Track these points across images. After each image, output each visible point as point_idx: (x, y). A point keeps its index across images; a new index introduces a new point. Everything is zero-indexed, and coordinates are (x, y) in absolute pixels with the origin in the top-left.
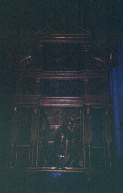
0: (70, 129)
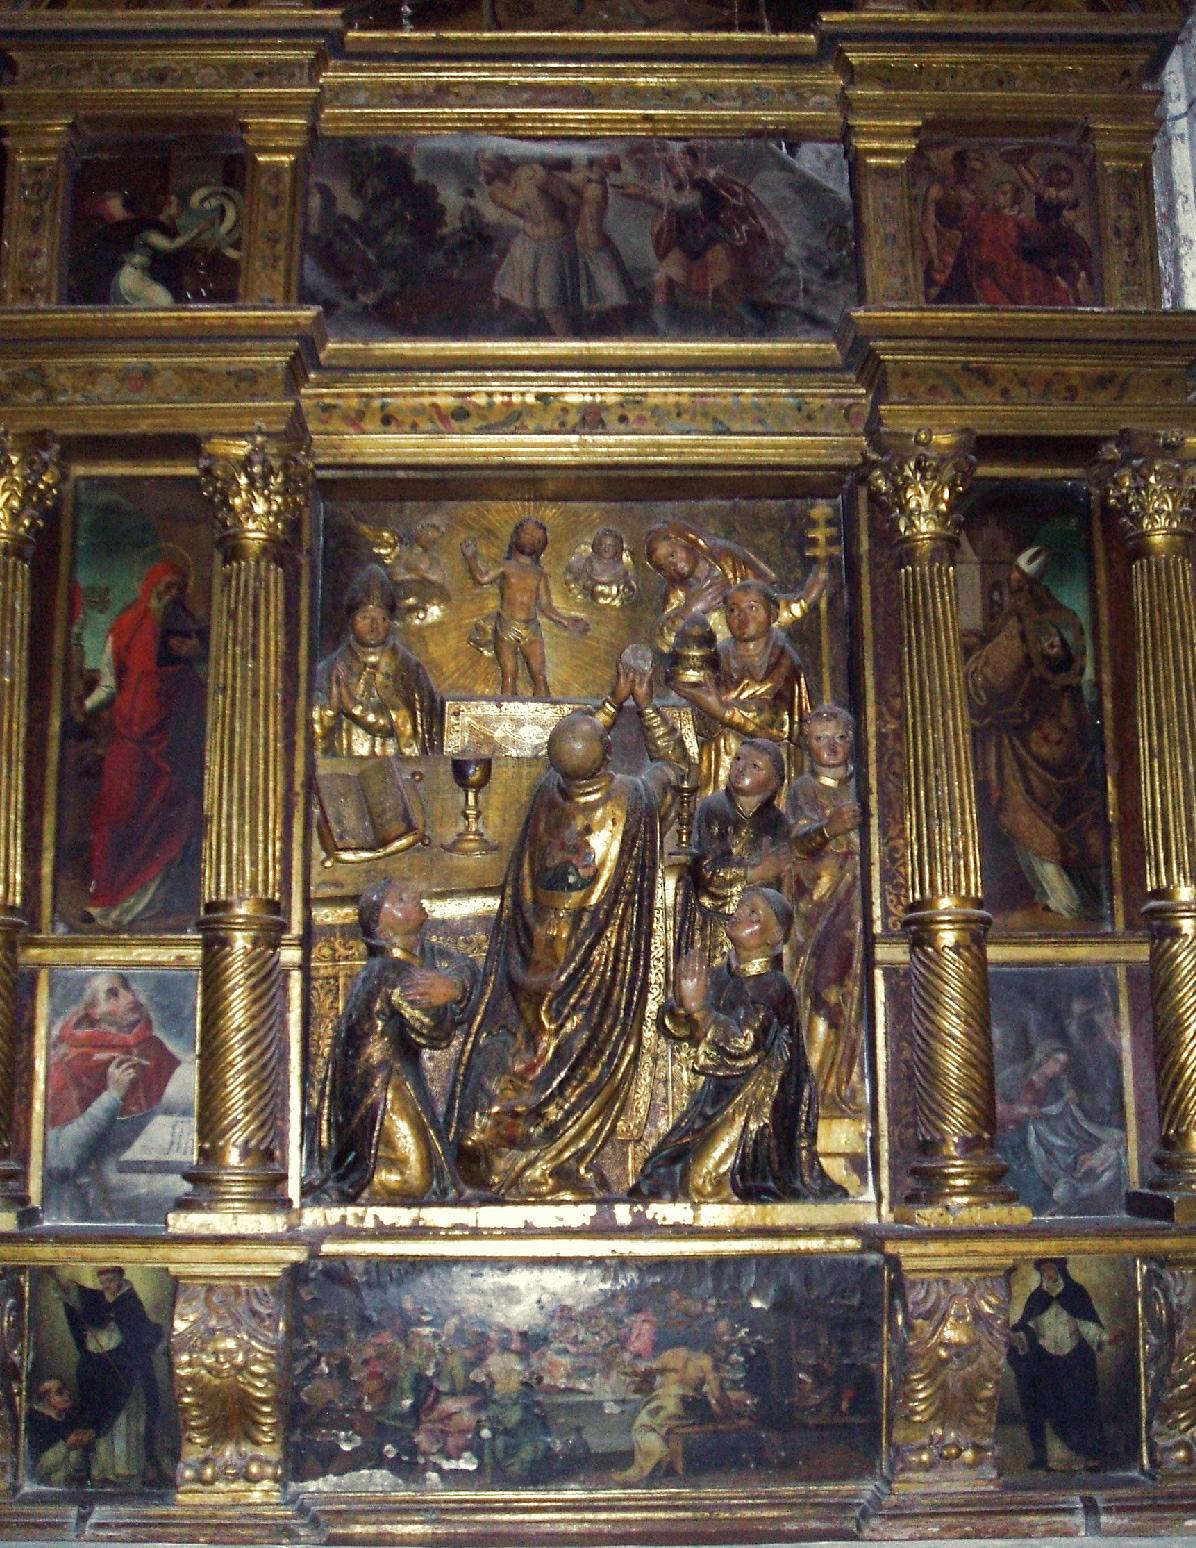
0: (692, 746)
